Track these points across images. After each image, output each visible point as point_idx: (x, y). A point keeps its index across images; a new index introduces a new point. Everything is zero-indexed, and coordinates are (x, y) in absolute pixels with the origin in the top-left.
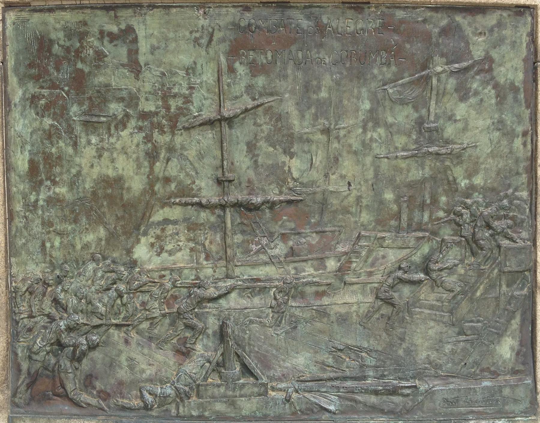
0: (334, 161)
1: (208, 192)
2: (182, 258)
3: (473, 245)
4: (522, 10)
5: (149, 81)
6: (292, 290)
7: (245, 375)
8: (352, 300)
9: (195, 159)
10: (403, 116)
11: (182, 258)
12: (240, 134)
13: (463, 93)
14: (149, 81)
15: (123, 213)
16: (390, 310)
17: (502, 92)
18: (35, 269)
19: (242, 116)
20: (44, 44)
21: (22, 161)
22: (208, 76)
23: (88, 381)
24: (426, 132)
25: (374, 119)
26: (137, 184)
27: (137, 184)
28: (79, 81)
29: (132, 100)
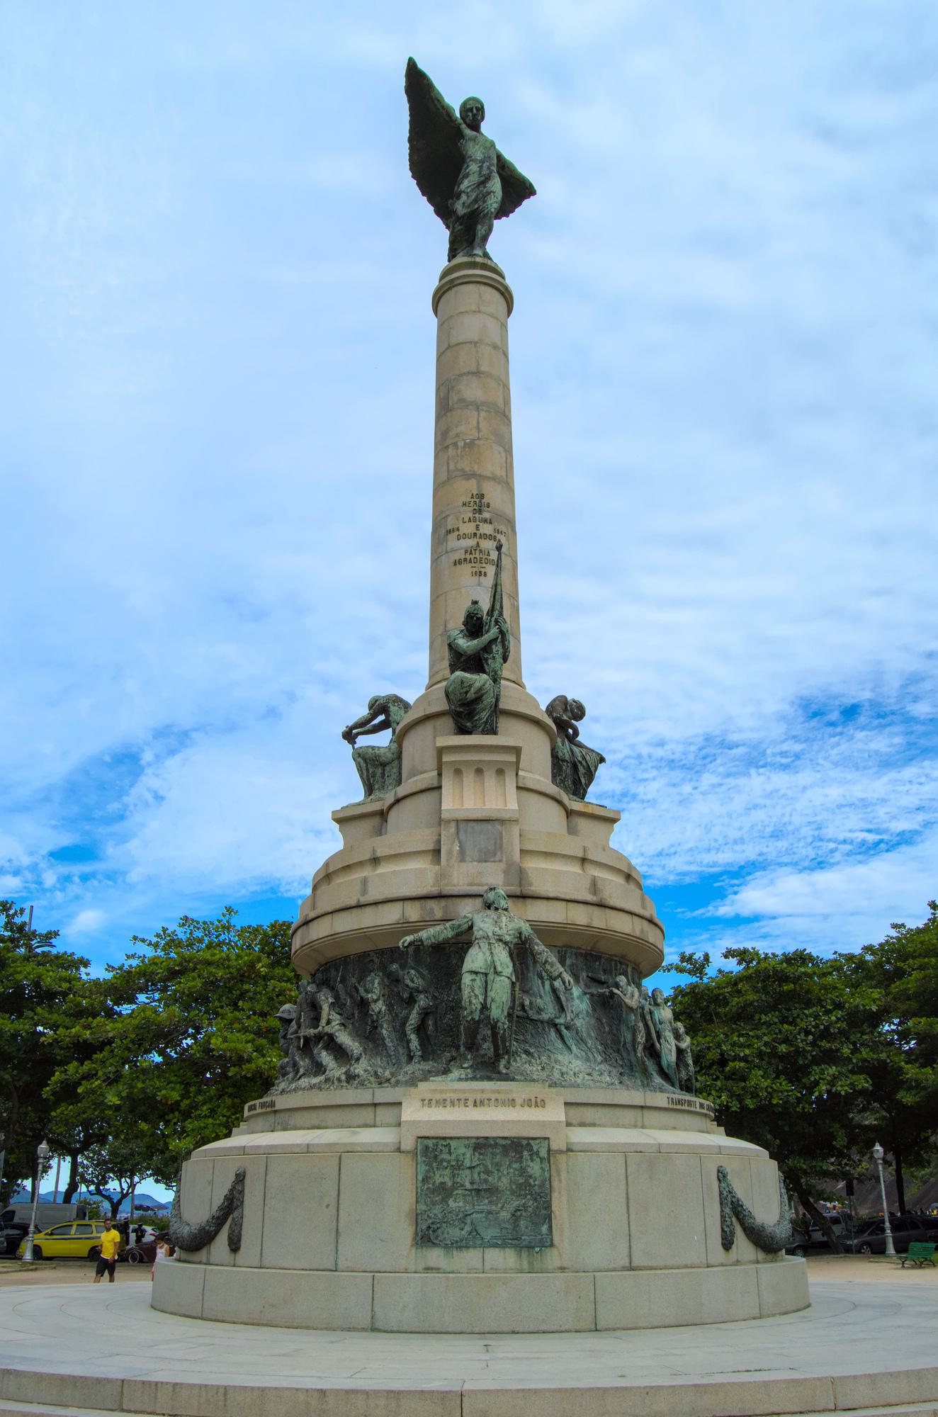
0: (500, 1178)
1: (468, 1186)
2: (461, 1204)
3: (535, 1200)
4: (545, 1139)
5: (453, 1157)
6: (490, 1212)
7: (465, 108)
8: (505, 1215)
9: (465, 1178)
10: (516, 1166)
11: (461, 1204)
12: (477, 1170)
13: (532, 1160)
14: (453, 1157)
15: (444, 1192)
16: (515, 1217)
17: (542, 1159)
18: (424, 1208)
19: (785, 859)
20: (427, 1147)
21: (420, 1178)
22: (468, 1155)
23: (437, 1237)
24: (523, 1171)
25: (510, 1166)
26: (450, 1184)
27: (450, 1184)
28: (436, 1157)
29: (449, 1162)
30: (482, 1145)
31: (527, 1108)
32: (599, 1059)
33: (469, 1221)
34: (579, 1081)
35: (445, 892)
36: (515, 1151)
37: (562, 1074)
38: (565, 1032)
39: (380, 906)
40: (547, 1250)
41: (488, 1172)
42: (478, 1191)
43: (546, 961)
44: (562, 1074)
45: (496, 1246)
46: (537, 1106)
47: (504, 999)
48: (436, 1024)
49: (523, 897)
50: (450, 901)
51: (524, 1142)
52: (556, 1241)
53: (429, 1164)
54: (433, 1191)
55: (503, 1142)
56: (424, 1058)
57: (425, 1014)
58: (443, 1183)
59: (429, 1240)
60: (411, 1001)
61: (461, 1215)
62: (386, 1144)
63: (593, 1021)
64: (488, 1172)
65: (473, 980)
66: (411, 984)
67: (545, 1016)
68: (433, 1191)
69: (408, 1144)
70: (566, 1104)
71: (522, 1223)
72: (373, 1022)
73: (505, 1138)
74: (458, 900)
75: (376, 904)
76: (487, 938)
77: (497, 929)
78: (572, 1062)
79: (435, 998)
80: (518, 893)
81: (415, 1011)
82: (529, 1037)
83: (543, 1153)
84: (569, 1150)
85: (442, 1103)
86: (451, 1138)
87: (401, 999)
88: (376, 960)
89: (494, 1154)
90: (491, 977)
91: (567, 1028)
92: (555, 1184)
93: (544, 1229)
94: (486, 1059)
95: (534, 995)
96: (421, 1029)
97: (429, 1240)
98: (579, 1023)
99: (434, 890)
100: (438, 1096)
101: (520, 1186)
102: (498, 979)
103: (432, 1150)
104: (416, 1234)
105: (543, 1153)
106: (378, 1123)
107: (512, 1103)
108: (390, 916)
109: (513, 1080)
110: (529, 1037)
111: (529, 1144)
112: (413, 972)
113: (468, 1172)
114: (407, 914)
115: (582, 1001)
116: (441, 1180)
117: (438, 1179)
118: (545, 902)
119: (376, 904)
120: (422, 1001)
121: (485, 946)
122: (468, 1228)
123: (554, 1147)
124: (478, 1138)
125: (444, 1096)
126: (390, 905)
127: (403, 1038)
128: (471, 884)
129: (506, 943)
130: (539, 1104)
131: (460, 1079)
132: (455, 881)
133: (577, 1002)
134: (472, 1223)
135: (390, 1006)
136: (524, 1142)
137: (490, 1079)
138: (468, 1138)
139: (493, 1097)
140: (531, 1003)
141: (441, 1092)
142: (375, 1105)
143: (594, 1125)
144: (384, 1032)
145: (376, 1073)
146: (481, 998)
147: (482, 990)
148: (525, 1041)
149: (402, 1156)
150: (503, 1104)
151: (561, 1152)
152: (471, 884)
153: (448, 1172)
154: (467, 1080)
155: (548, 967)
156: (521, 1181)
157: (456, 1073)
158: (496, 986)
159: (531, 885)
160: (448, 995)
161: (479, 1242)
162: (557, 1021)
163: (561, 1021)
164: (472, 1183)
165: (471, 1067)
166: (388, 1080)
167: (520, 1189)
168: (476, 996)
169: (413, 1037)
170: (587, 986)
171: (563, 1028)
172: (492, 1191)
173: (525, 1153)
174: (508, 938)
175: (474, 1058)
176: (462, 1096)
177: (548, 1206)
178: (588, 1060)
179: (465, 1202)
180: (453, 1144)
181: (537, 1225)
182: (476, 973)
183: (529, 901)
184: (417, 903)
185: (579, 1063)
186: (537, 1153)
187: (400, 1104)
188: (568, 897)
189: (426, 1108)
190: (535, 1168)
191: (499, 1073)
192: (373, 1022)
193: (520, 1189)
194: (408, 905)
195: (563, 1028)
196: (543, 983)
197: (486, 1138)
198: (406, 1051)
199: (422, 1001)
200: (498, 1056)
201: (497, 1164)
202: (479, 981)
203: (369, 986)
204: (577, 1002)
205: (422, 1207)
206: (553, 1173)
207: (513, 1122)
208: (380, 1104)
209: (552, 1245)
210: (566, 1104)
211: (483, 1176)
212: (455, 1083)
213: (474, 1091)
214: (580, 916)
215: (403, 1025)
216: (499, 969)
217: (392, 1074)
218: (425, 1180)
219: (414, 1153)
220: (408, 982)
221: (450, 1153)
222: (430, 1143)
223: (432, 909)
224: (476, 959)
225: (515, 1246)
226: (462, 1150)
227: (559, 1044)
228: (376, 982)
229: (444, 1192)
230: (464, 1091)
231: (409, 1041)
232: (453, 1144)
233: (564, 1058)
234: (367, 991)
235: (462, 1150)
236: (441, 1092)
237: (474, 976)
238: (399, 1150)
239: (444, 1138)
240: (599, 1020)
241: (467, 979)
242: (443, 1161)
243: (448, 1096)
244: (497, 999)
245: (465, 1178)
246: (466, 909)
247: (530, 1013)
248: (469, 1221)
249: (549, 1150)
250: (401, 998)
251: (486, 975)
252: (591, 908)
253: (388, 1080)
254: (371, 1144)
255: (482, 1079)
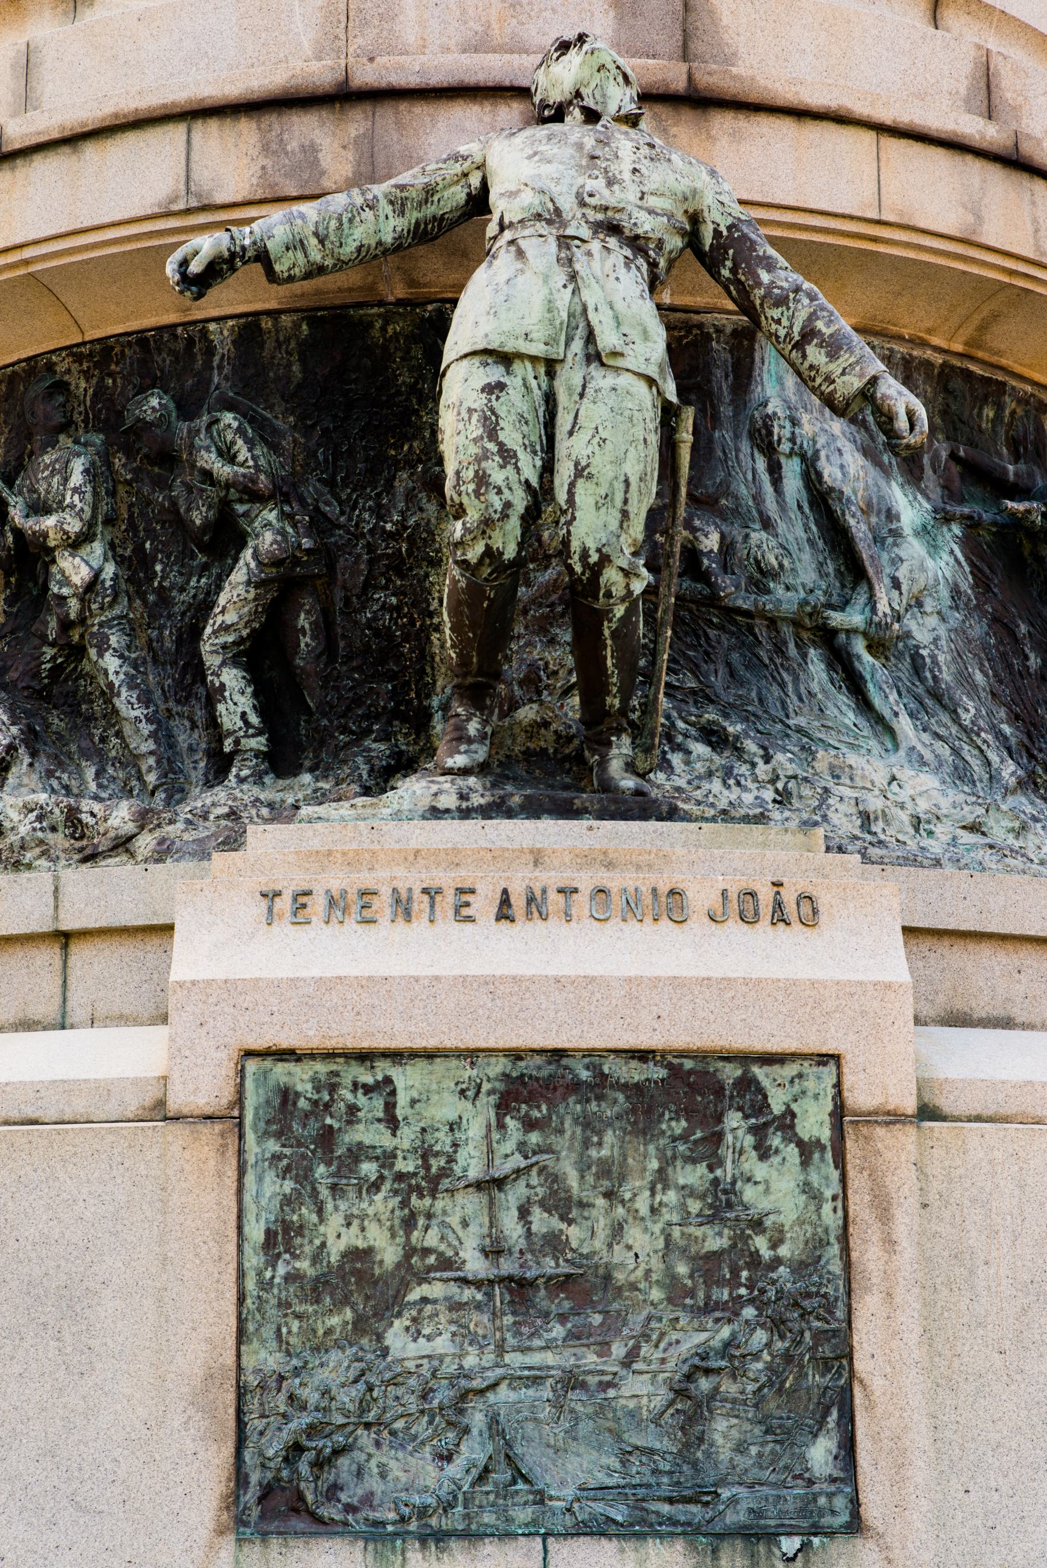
0: (617, 1230)
1: (475, 1265)
2: (442, 1344)
3: (777, 1325)
4: (824, 1059)
5: (407, 1137)
6: (571, 1381)
8: (643, 1391)
9: (461, 1227)
10: (694, 1175)
11: (442, 1344)
12: (513, 1196)
14: (407, 1137)
15: (367, 1291)
16: (690, 1402)
17: (807, 1150)
20: (286, 1096)
21: (256, 1232)
22: (475, 1130)
23: (333, 1491)
24: (721, 1202)
25: (662, 1179)
26: (390, 1255)
27: (390, 1255)
28: (327, 1138)
29: (387, 1158)
30: (535, 1086)
31: (734, 927)
32: (1009, 771)
33: (477, 1419)
34: (935, 847)
35: (366, 76)
36: (688, 1112)
37: (866, 819)
38: (866, 661)
39: (91, 151)
40: (838, 1546)
41: (561, 1204)
42: (520, 1288)
43: (809, 334)
44: (866, 819)
45: (598, 1529)
46: (779, 917)
47: (632, 469)
48: (325, 628)
49: (698, 101)
50: (386, 115)
51: (730, 1073)
52: (872, 1510)
53: (296, 1170)
54: (316, 1289)
55: (635, 1073)
56: (280, 762)
57: (281, 585)
58: (360, 1257)
59: (298, 1506)
60: (225, 539)
61: (443, 1395)
62: (104, 1089)
63: (978, 629)
64: (561, 1204)
65: (495, 389)
66: (223, 470)
67: (784, 599)
68: (316, 1289)
69: (205, 1086)
70: (908, 931)
71: (723, 1431)
72: (66, 625)
73: (643, 1055)
74: (421, 110)
75: (73, 140)
76: (555, 217)
77: (598, 184)
78: (903, 776)
79: (320, 525)
80: (679, 84)
81: (239, 575)
82: (718, 680)
83: (814, 1123)
84: (927, 1113)
85: (356, 906)
86: (396, 1056)
87: (168, 536)
88: (81, 385)
89: (589, 1125)
90: (570, 376)
91: (876, 647)
92: (868, 1254)
93: (821, 1453)
94: (546, 741)
95: (736, 514)
96: (262, 652)
97: (298, 1506)
98: (923, 630)
99: (320, 72)
100: (336, 880)
101: (708, 1265)
102: (602, 380)
103: (305, 1114)
104: (240, 1477)
105: (814, 1123)
106: (78, 1012)
107: (672, 905)
108: (133, 182)
109: (672, 814)
110: (718, 680)
111: (747, 1084)
112: (229, 418)
113: (471, 1203)
114: (202, 176)
115: (934, 548)
116: (352, 1238)
117: (337, 1236)
118: (786, 126)
119: (73, 140)
120: (267, 532)
121: (542, 250)
122: (474, 1451)
123: (861, 1096)
124: (516, 1055)
125: (366, 879)
126: (131, 140)
127: (186, 682)
128: (478, 46)
129: (636, 243)
130: (790, 910)
131: (435, 813)
132: (411, 37)
133: (913, 548)
134: (493, 1421)
135: (135, 567)
136: (730, 1073)
137: (567, 811)
138: (471, 1055)
139: (585, 881)
140: (727, 547)
141: (352, 861)
142: (65, 938)
143: (1007, 1023)
144: (111, 663)
145: (72, 817)
146: (529, 467)
147: (536, 433)
148: (704, 696)
149: (176, 1134)
150: (631, 908)
151: (894, 1118)
152: (478, 46)
153: (382, 1203)
154: (465, 814)
155: (815, 355)
156: (715, 1241)
157: (412, 790)
158: (592, 413)
159: (730, 59)
160: (380, 513)
161: (523, 1515)
162: (836, 619)
163: (854, 617)
164: (493, 1251)
165: (482, 769)
166: (123, 845)
167: (711, 1279)
168: (507, 456)
169: (231, 678)
170: (950, 493)
171: (859, 646)
172: (584, 1287)
173: (733, 1120)
174: (647, 225)
175: (493, 739)
176: (447, 879)
177: (838, 1354)
178: (961, 774)
179: (465, 1336)
180: (407, 1080)
181: (785, 1436)
182: (505, 359)
183: (723, 122)
184: (247, 129)
185: (929, 781)
186: (787, 1122)
187: (168, 929)
188: (885, 115)
189: (283, 929)
190: (775, 1187)
191: (607, 787)
192: (66, 625)
193: (711, 1279)
194: (210, 137)
195: (859, 646)
196: (775, 470)
197: (558, 1054)
198: (200, 739)
199: (267, 532)
200: (599, 725)
201: (605, 1169)
202: (518, 400)
203: (46, 484)
204: (913, 548)
205: (263, 1357)
206: (859, 1203)
207: (676, 983)
208: (85, 934)
209: (855, 1525)
210: (908, 931)
211: (541, 1221)
212: (406, 829)
213: (496, 856)
214: (934, 196)
215: (191, 636)
216: (607, 339)
217: (143, 819)
218: (280, 1239)
219: (230, 1118)
220: (210, 460)
221: (392, 1122)
222: (301, 1077)
223: (311, 150)
224: (496, 304)
225: (690, 1531)
226: (446, 1107)
227: (843, 710)
228: (78, 466)
229: (367, 1291)
230: (453, 858)
231: (214, 695)
232: (407, 1080)
233: (870, 764)
234: (39, 508)
235: (446, 1107)
236: (352, 861)
237: (495, 373)
238: (160, 1112)
239: (365, 1057)
240: (1000, 624)
241: (461, 386)
242: (358, 1153)
243: (382, 878)
244: (602, 466)
245: (461, 1227)
246: (443, 146)
247: (726, 584)
248: (477, 1419)
249: (839, 1112)
250: (177, 521)
251: (551, 366)
252: (975, 166)
253: (123, 845)
254: (37, 1090)
255: (532, 810)
